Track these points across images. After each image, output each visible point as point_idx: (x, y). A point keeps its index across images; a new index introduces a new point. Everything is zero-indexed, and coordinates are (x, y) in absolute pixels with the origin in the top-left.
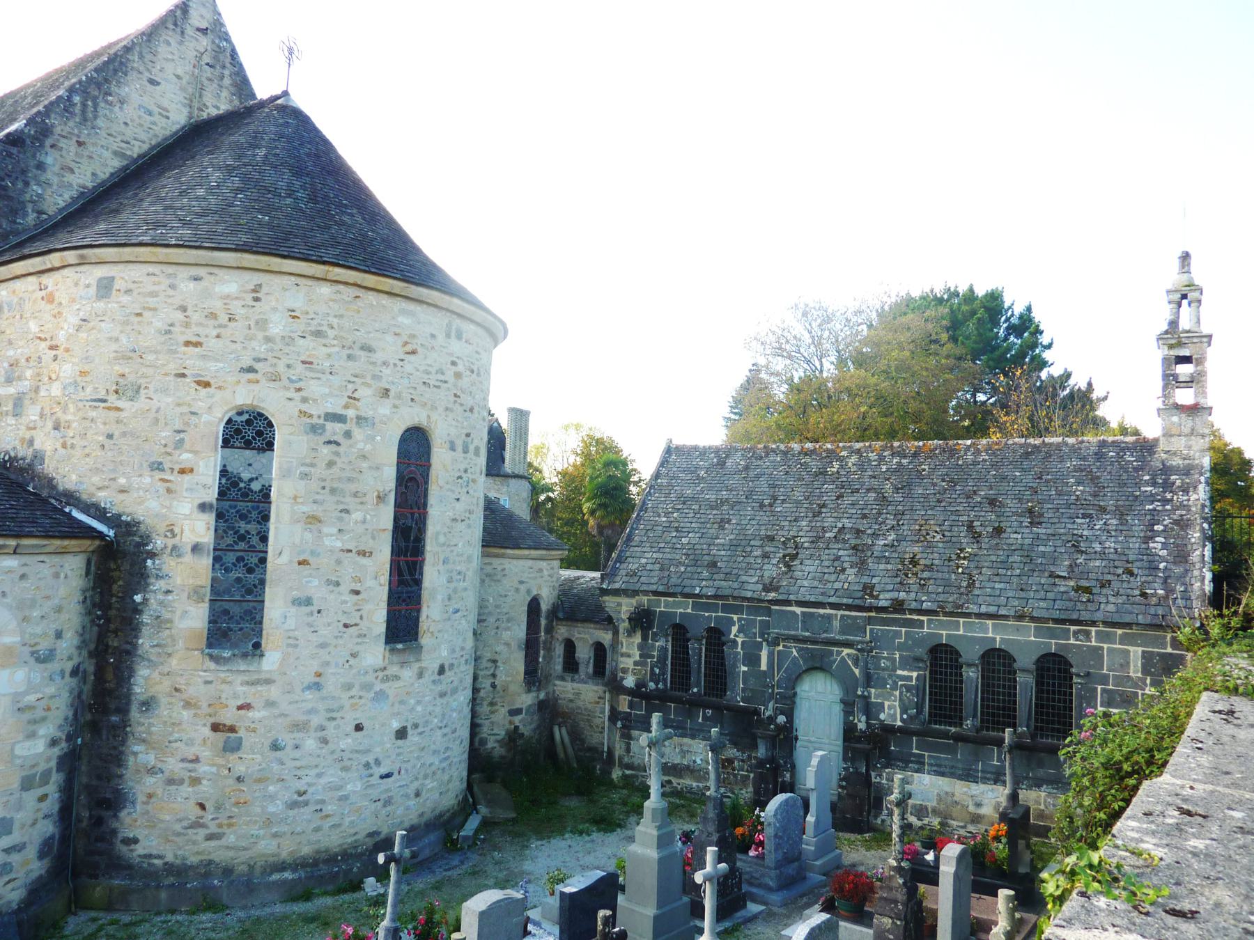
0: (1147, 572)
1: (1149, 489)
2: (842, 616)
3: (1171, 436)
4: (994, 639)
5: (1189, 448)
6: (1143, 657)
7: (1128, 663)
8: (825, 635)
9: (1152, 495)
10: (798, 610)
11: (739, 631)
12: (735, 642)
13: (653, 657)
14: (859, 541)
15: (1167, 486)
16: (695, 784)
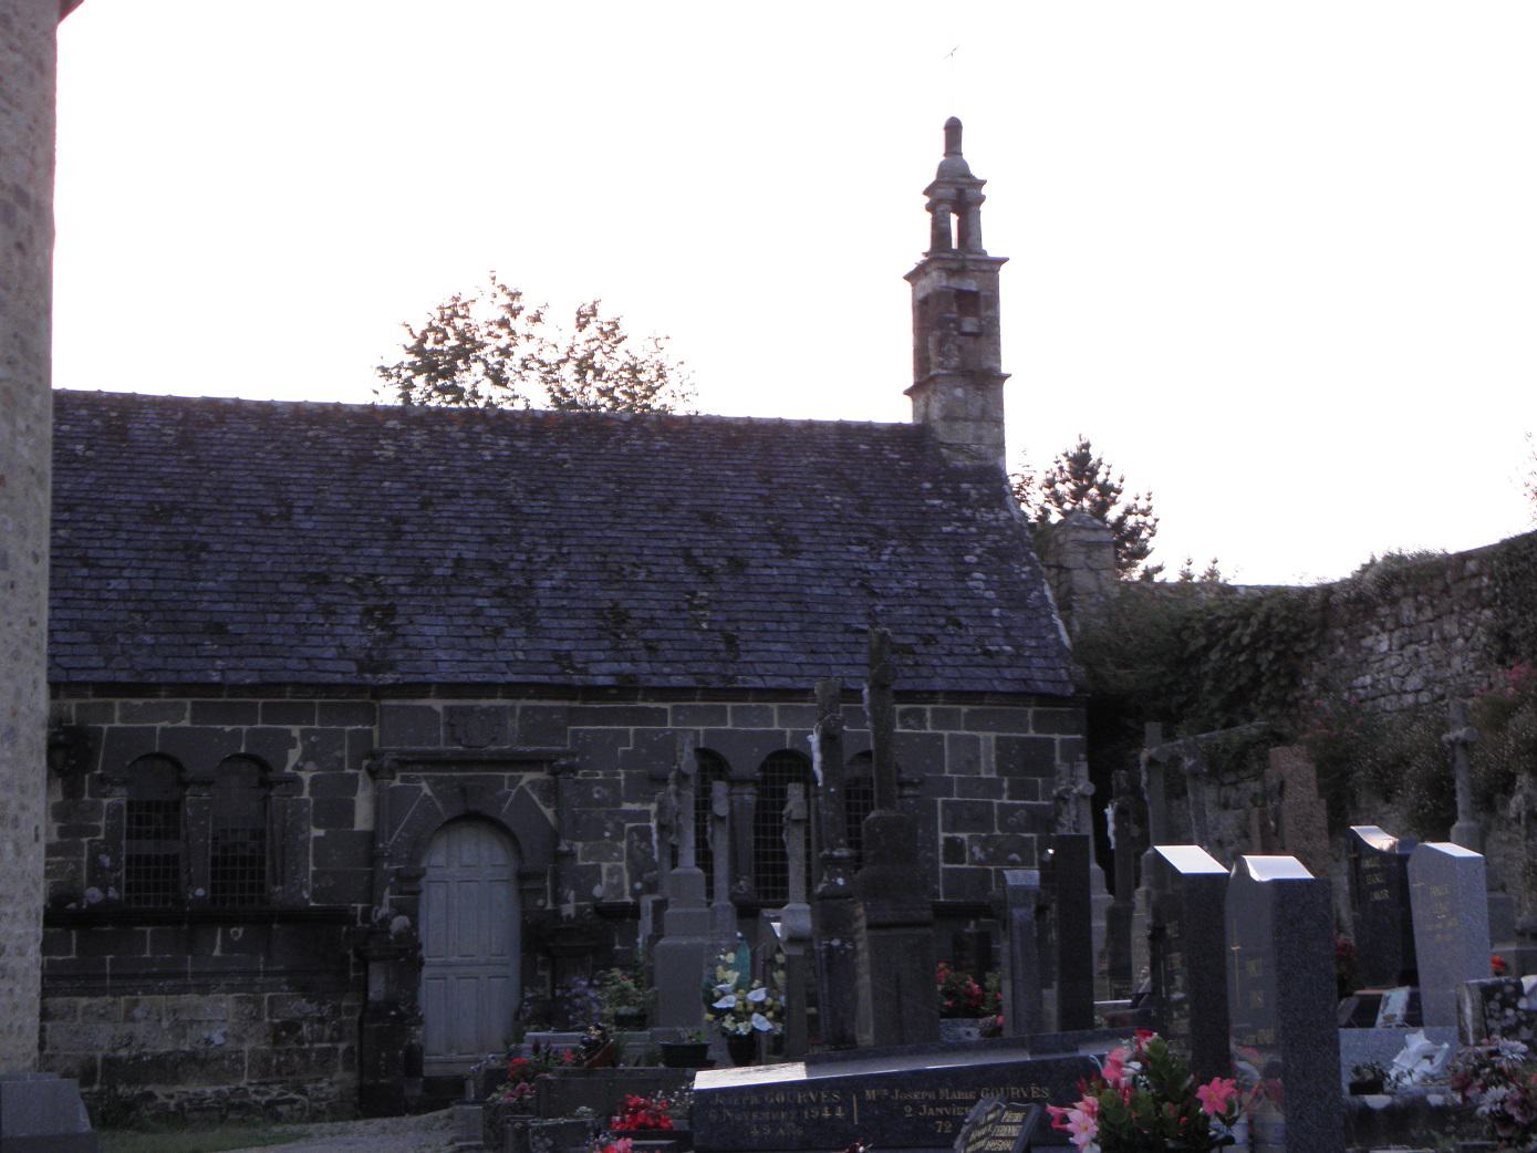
0: (978, 621)
1: (937, 502)
2: (525, 709)
3: (956, 419)
4: (782, 734)
5: (979, 439)
6: (998, 747)
7: (978, 758)
8: (493, 748)
9: (944, 512)
10: (438, 705)
11: (305, 758)
12: (294, 781)
13: (96, 831)
14: (504, 582)
15: (961, 499)
16: (209, 1090)
